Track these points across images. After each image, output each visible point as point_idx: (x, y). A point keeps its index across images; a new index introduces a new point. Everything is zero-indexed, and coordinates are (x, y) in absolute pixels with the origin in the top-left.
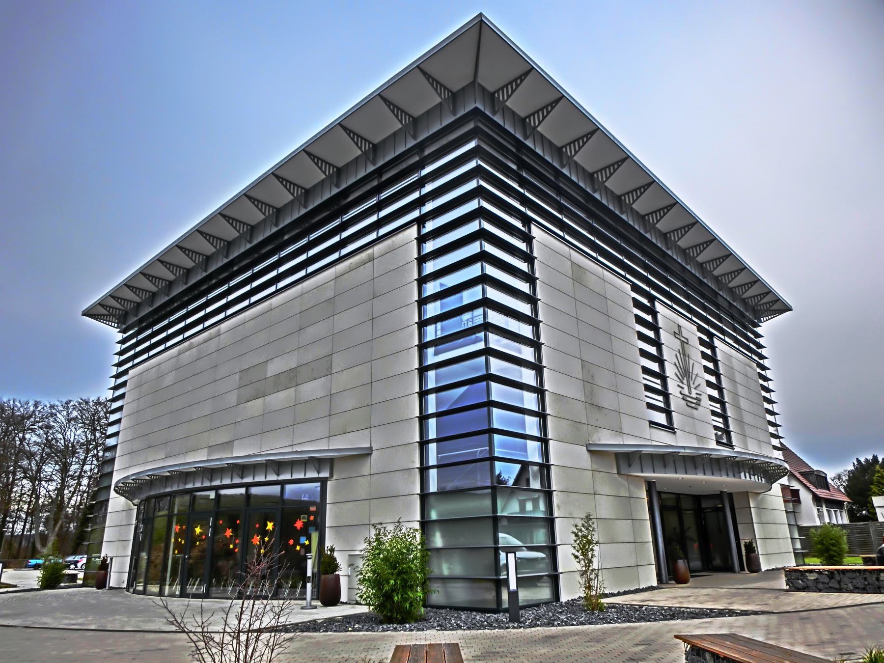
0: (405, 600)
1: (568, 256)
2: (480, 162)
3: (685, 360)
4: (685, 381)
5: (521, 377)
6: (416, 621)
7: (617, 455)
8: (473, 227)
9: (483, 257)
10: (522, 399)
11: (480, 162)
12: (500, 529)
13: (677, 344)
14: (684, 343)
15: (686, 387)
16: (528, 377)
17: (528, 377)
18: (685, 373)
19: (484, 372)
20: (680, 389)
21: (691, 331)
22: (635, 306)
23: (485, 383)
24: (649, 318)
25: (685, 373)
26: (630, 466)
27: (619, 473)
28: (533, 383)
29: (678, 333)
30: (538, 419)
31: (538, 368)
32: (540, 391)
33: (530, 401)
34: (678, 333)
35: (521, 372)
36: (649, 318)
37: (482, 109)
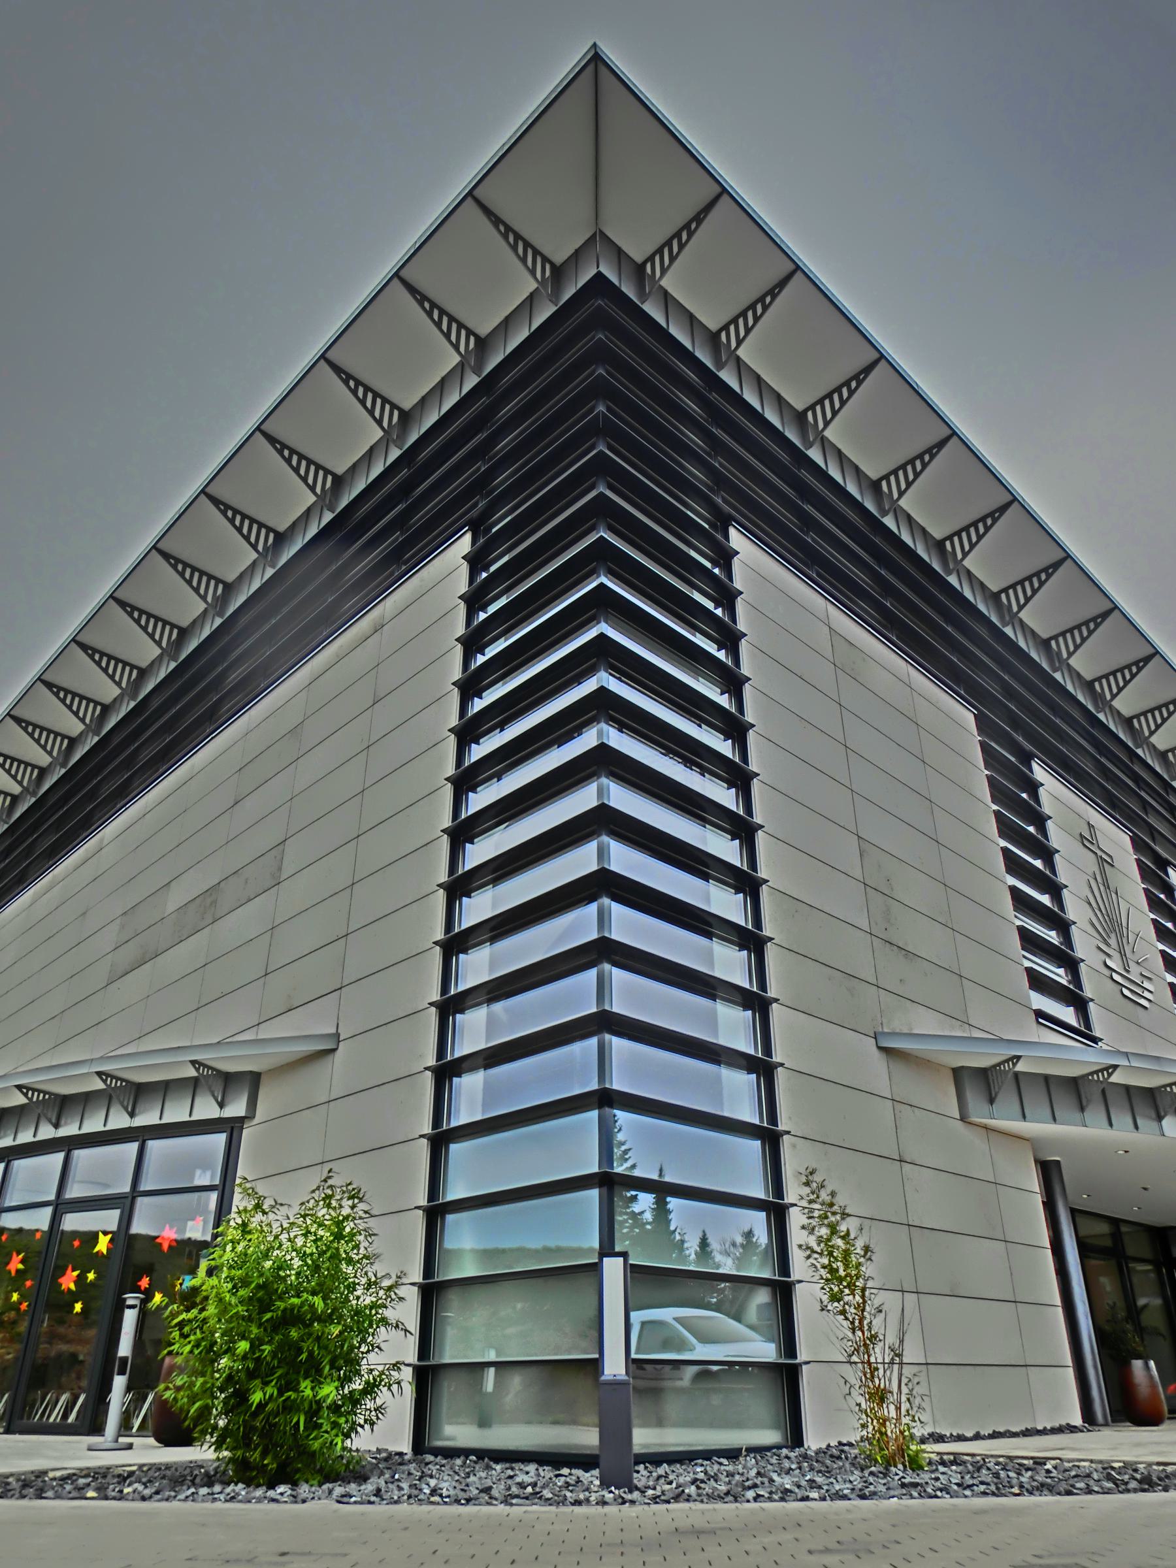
0: (289, 1408)
1: (823, 616)
2: (603, 579)
3: (1111, 902)
4: (1113, 941)
5: (711, 964)
6: (329, 1476)
7: (958, 1074)
8: (580, 801)
9: (605, 820)
10: (712, 1022)
11: (603, 579)
12: (635, 1421)
13: (1090, 863)
14: (1105, 862)
15: (1116, 955)
16: (732, 1027)
17: (732, 1027)
18: (1112, 927)
19: (594, 1086)
20: (1103, 957)
21: (1117, 840)
22: (1010, 870)
23: (593, 1041)
24: (1052, 936)
25: (1112, 927)
26: (991, 1101)
27: (963, 1118)
28: (745, 1045)
29: (1088, 840)
30: (764, 1214)
31: (757, 1003)
32: (762, 1068)
33: (738, 1096)
34: (1088, 840)
35: (719, 1078)
36: (1052, 936)
37: (614, 279)
